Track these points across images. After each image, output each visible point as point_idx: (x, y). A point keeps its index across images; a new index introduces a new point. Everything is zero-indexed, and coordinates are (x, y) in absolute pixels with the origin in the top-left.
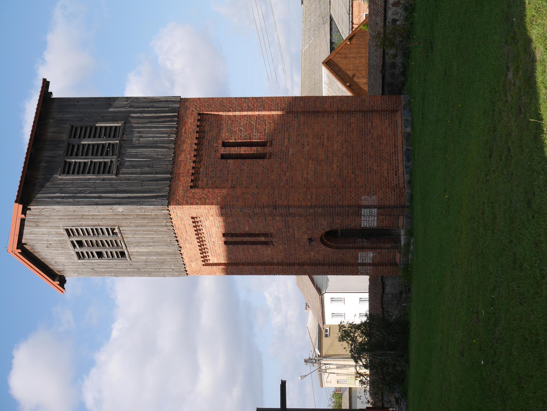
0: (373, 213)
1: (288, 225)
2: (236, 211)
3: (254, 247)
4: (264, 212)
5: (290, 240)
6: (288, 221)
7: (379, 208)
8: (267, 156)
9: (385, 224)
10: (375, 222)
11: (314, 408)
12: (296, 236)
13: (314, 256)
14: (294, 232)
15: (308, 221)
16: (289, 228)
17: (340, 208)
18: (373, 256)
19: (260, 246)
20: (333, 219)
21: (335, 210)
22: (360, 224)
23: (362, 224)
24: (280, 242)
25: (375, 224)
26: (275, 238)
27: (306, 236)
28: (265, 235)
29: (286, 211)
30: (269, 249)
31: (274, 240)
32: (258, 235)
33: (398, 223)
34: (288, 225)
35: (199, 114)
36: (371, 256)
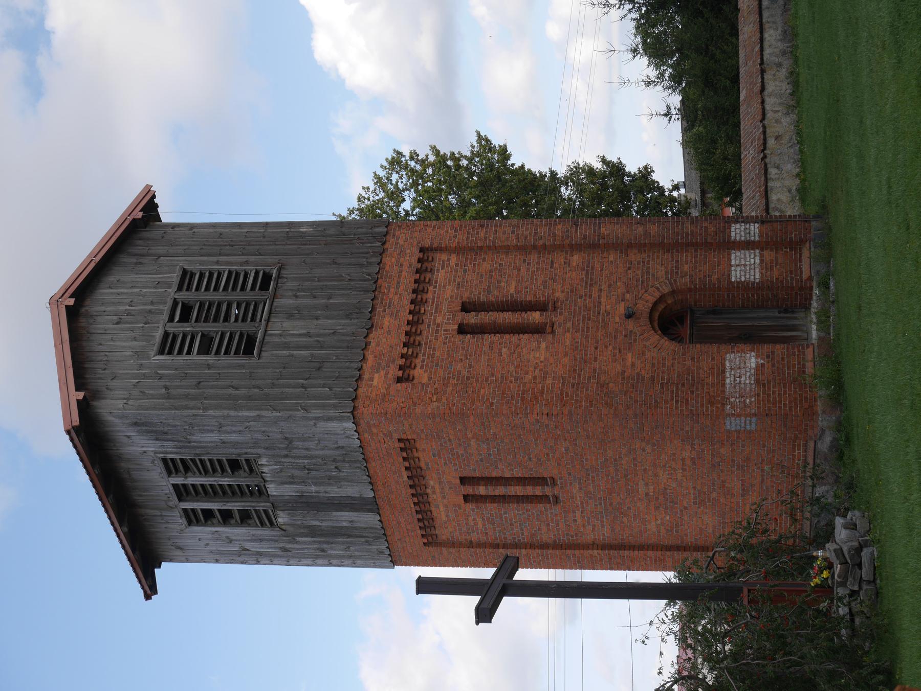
0: (752, 233)
1: (592, 280)
2: (504, 233)
3: (514, 338)
4: (554, 233)
5: (589, 319)
6: (593, 268)
7: (762, 223)
8: (548, 329)
9: (776, 273)
10: (757, 270)
11: (631, 601)
12: (603, 307)
13: (633, 365)
14: (599, 297)
15: (629, 268)
16: (591, 285)
17: (692, 223)
18: (757, 364)
19: (526, 336)
20: (677, 262)
21: (682, 229)
22: (729, 276)
23: (733, 273)
24: (569, 325)
25: (758, 276)
26: (561, 314)
27: (622, 308)
28: (541, 307)
29: (595, 232)
30: (543, 345)
31: (557, 318)
32: (494, 499)
33: (801, 272)
34: (592, 280)
35: (400, 440)
36: (753, 365)
